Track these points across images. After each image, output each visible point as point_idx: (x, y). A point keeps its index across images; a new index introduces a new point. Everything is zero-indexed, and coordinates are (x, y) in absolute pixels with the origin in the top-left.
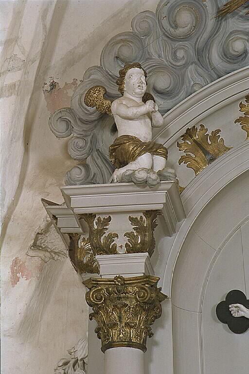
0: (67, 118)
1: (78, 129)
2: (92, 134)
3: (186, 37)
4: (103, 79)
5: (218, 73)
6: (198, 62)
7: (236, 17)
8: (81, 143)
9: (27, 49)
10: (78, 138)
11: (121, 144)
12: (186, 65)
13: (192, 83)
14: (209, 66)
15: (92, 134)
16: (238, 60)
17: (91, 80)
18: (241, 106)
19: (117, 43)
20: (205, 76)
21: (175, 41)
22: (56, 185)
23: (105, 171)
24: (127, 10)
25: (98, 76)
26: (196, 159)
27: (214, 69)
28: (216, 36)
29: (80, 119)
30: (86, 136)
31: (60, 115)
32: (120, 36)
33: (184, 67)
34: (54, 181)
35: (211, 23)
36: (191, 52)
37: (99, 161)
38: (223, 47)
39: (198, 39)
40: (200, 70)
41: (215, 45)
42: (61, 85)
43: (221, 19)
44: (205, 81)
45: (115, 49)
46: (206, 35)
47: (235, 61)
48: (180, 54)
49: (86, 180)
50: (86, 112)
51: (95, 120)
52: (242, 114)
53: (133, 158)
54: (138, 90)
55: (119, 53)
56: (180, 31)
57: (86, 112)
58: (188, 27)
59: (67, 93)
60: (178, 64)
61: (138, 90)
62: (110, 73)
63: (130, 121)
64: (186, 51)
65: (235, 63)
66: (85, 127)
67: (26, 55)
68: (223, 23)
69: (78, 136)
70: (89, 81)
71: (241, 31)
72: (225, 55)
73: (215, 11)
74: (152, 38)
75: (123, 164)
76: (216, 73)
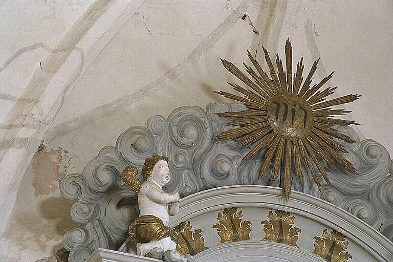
0: (79, 183)
1: (85, 196)
2: (96, 204)
3: (187, 147)
4: (117, 159)
5: (205, 183)
6: (191, 169)
7: (224, 144)
8: (86, 209)
9: (46, 112)
10: (84, 204)
11: (150, 222)
12: (183, 169)
13: (184, 185)
14: (199, 175)
15: (96, 204)
16: (220, 178)
17: (107, 157)
18: (219, 215)
19: (135, 133)
20: (196, 182)
21: (178, 146)
22: (34, 240)
23: (102, 239)
24: (115, 105)
25: (113, 156)
26: (182, 250)
27: (203, 178)
28: (207, 154)
29: (89, 188)
30: (90, 204)
31: (74, 179)
32: (138, 128)
33: (181, 170)
34: (32, 235)
35: (207, 142)
36: (188, 159)
37: (99, 230)
38: (212, 164)
39: (195, 151)
40: (193, 177)
41: (207, 160)
42: (48, 150)
43: (214, 142)
44: (194, 186)
45: (134, 138)
46: (202, 150)
47: (219, 178)
48: (181, 158)
49: (83, 244)
50: (98, 183)
51: (102, 192)
52: (218, 222)
53: (158, 237)
54: (165, 180)
55: (137, 142)
56: (184, 140)
57: (98, 183)
58: (192, 140)
59: (51, 158)
60: (178, 166)
61: (165, 180)
62: (124, 156)
63: (158, 205)
64: (185, 158)
65: (219, 179)
66: (93, 196)
67: (44, 117)
68: (215, 145)
69: (84, 202)
70: (105, 157)
71: (226, 156)
72: (212, 170)
73: (211, 134)
74: (162, 138)
75: (146, 241)
76: (203, 182)
